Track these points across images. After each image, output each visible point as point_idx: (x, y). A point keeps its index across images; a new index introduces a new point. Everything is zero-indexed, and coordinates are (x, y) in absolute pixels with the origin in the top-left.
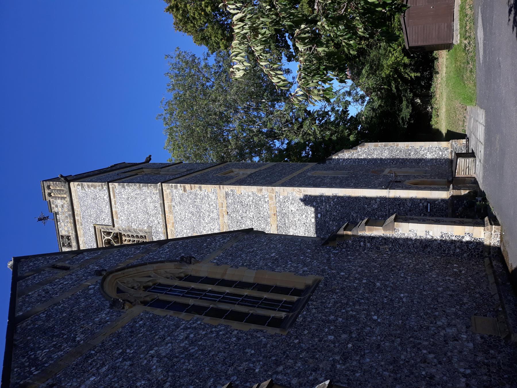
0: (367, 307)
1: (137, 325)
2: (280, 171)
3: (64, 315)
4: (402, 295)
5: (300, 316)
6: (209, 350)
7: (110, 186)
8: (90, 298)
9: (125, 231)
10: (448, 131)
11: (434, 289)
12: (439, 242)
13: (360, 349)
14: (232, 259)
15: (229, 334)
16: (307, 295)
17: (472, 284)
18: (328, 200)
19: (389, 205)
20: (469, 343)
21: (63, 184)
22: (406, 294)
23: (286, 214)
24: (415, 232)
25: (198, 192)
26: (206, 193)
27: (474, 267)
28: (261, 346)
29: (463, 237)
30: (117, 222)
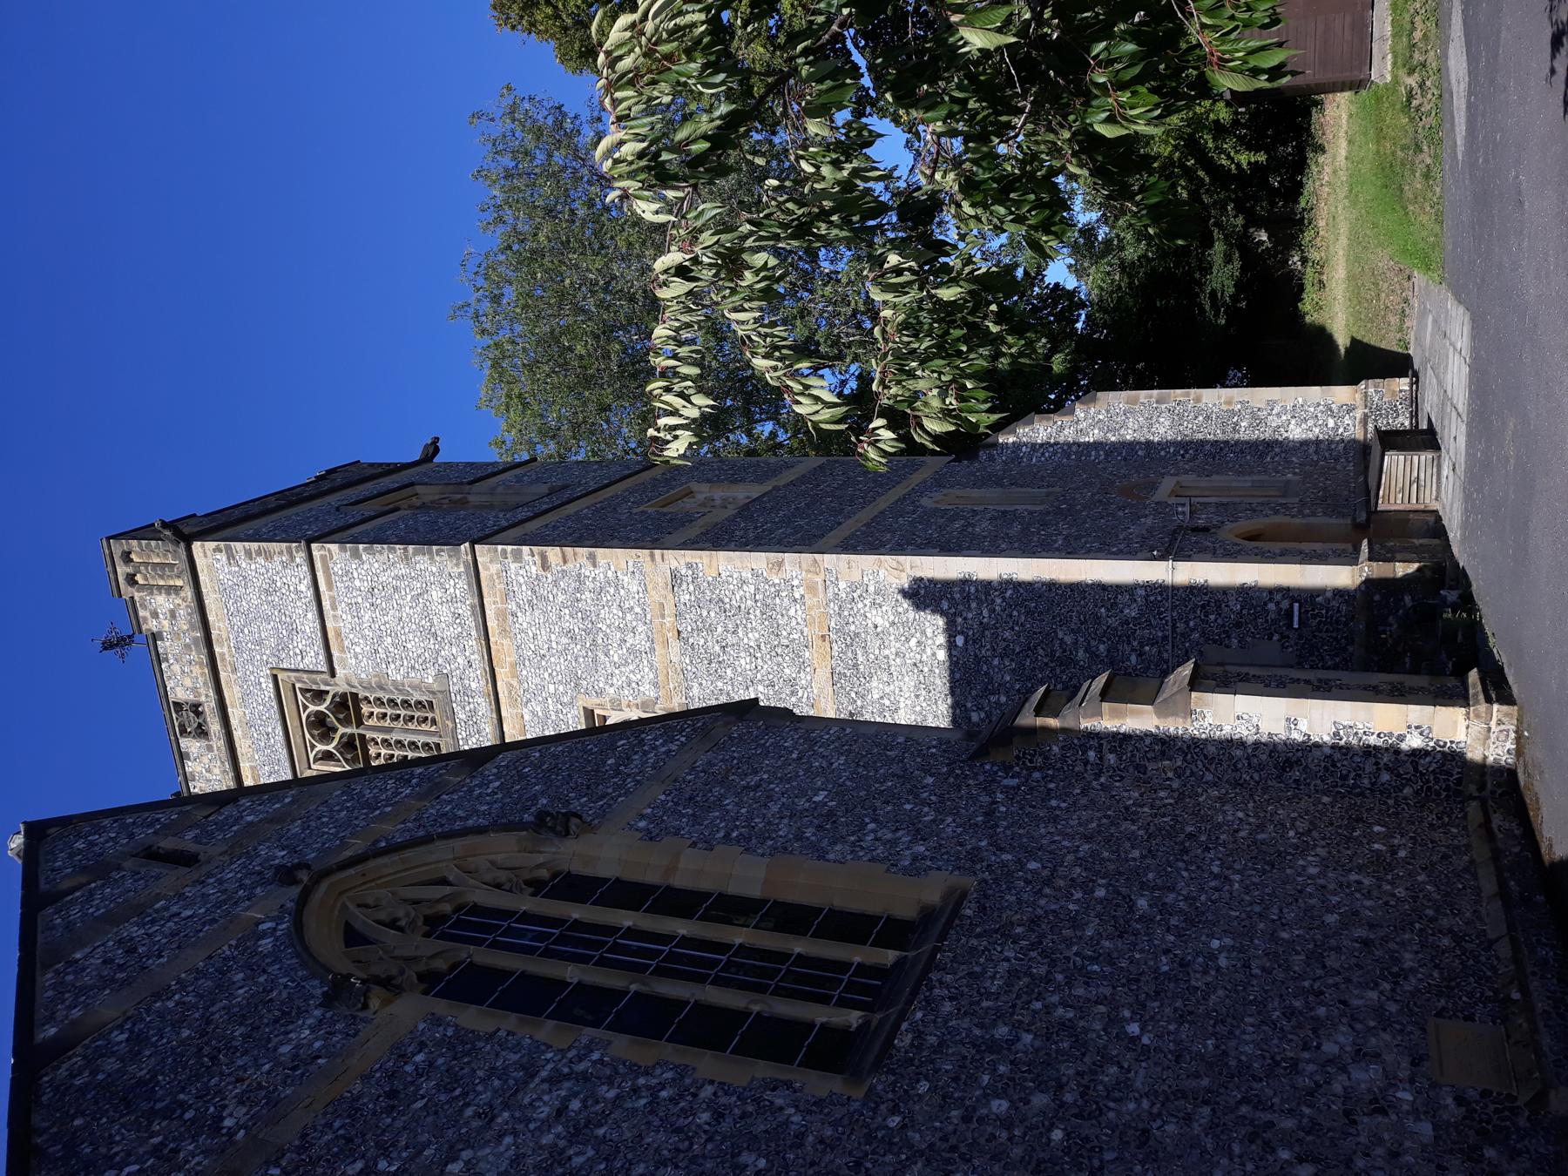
0: (1107, 991)
1: (409, 1068)
2: (838, 493)
3: (186, 1033)
4: (1215, 944)
5: (904, 1026)
6: (630, 1156)
7: (316, 554)
8: (264, 971)
9: (368, 688)
10: (1354, 341)
11: (1312, 918)
12: (1328, 751)
13: (1088, 1146)
14: (694, 815)
15: (689, 1098)
16: (927, 947)
17: (1429, 900)
18: (987, 594)
19: (1174, 607)
20: (1420, 1120)
21: (171, 547)
22: (1228, 941)
23: (857, 635)
24: (1255, 720)
25: (588, 570)
26: (610, 574)
27: (1437, 835)
28: (789, 1143)
29: (1401, 738)
30: (342, 660)
